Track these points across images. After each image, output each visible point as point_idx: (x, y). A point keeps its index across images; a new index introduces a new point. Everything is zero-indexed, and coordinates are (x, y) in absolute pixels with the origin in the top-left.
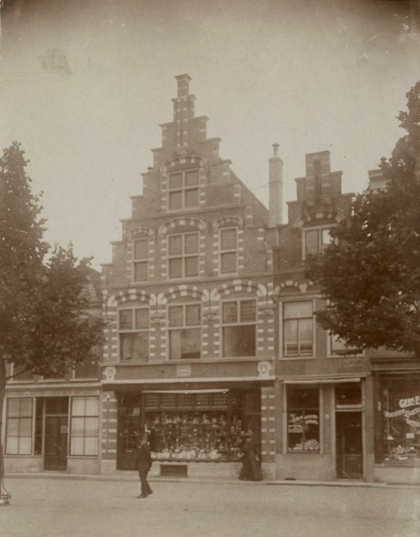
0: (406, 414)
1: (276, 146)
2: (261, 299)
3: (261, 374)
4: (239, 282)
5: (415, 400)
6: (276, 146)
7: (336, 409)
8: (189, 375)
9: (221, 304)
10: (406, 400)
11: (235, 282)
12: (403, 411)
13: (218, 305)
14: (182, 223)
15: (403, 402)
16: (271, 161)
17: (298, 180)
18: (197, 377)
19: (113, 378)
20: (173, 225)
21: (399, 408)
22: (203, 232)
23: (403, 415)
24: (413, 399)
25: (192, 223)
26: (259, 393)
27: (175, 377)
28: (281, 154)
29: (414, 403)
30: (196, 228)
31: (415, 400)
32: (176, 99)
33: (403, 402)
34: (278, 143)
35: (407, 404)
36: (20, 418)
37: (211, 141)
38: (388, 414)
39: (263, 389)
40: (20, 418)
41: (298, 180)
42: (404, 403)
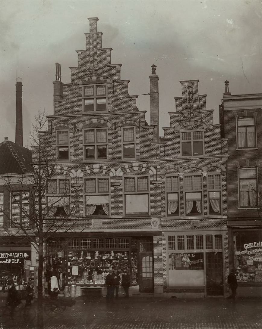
0: (248, 253)
1: (154, 67)
2: (153, 176)
3: (153, 227)
4: (137, 164)
5: (254, 244)
6: (154, 67)
7: (63, 294)
8: (102, 226)
9: (123, 178)
10: (248, 244)
11: (134, 164)
12: (246, 251)
13: (122, 179)
14: (95, 121)
15: (246, 245)
16: (151, 77)
17: (176, 98)
18: (107, 228)
19: (157, 227)
20: (87, 122)
21: (244, 249)
22: (110, 129)
23: (246, 253)
24: (252, 243)
25: (102, 122)
26: (152, 240)
27: (91, 228)
28: (158, 73)
29: (254, 246)
30: (105, 125)
31: (254, 244)
32: (89, 34)
33: (246, 245)
34: (155, 65)
35: (249, 246)
36: (220, 231)
37: (115, 66)
38: (237, 253)
39: (155, 237)
40: (220, 231)
41: (176, 98)
42: (247, 246)
